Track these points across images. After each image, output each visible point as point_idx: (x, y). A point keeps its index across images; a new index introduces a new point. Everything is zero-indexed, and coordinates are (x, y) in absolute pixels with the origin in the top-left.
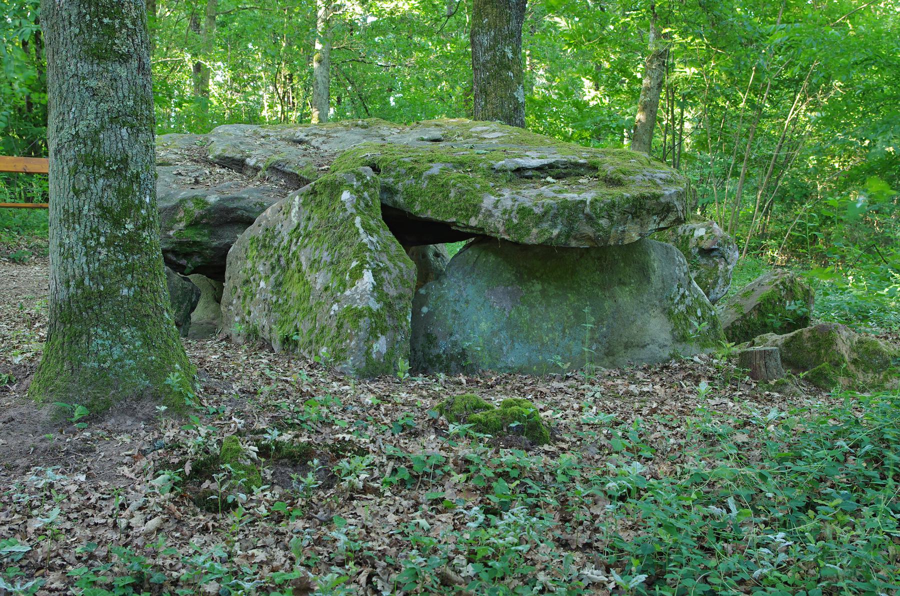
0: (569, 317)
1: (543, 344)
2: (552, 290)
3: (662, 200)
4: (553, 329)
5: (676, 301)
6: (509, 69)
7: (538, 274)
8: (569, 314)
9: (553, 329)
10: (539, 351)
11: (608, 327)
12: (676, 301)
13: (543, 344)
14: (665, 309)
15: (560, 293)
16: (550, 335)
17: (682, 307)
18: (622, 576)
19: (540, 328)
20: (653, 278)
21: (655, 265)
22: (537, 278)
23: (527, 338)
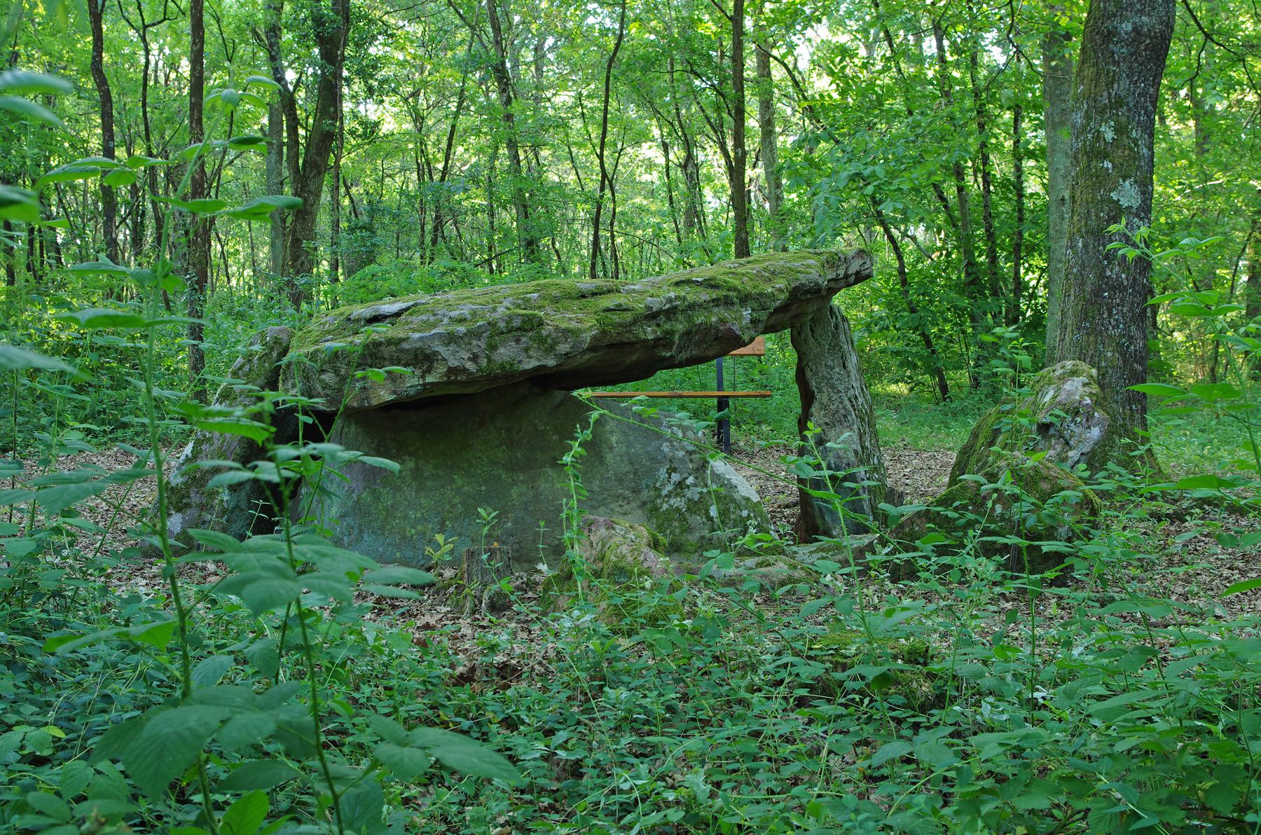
0: (453, 506)
1: (404, 538)
2: (428, 470)
3: (405, 346)
4: (423, 520)
5: (664, 492)
6: (1105, 158)
7: (411, 449)
8: (455, 501)
9: (423, 520)
10: (398, 547)
11: (516, 522)
12: (664, 492)
13: (404, 538)
14: (644, 504)
15: (441, 473)
16: (419, 528)
17: (677, 502)
18: (151, 545)
19: (405, 517)
20: (609, 458)
21: (614, 439)
22: (410, 454)
23: (382, 528)
